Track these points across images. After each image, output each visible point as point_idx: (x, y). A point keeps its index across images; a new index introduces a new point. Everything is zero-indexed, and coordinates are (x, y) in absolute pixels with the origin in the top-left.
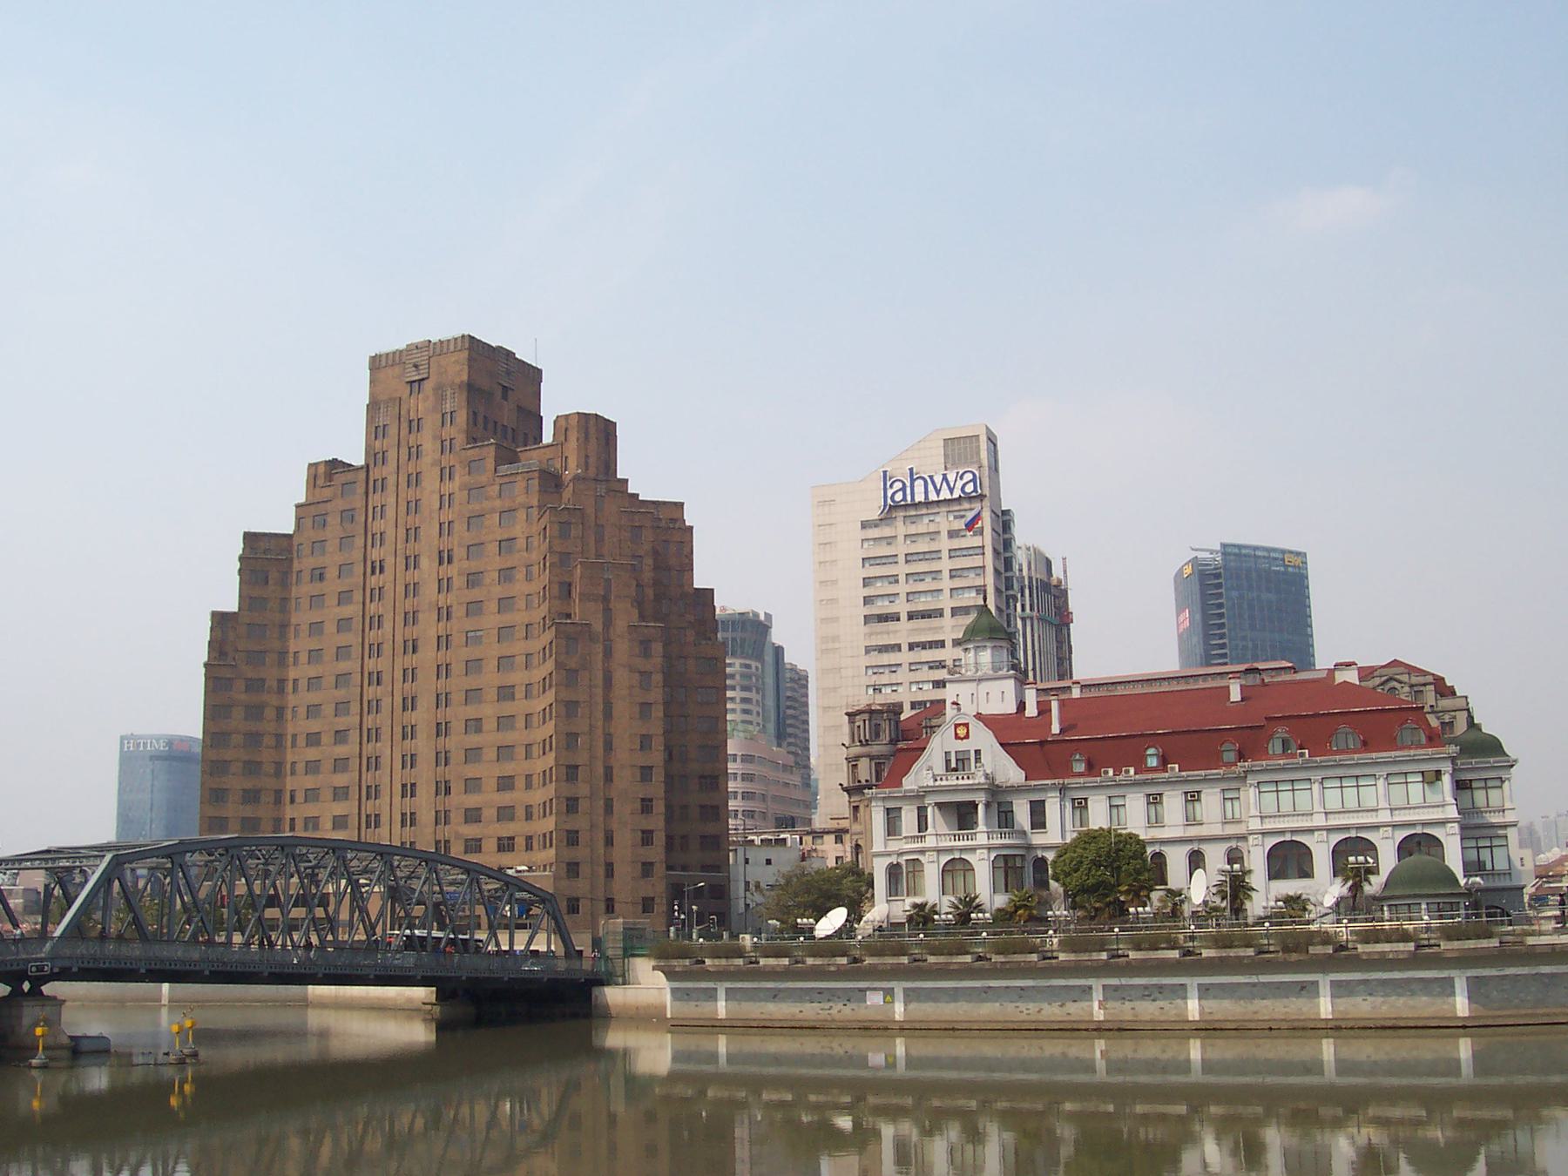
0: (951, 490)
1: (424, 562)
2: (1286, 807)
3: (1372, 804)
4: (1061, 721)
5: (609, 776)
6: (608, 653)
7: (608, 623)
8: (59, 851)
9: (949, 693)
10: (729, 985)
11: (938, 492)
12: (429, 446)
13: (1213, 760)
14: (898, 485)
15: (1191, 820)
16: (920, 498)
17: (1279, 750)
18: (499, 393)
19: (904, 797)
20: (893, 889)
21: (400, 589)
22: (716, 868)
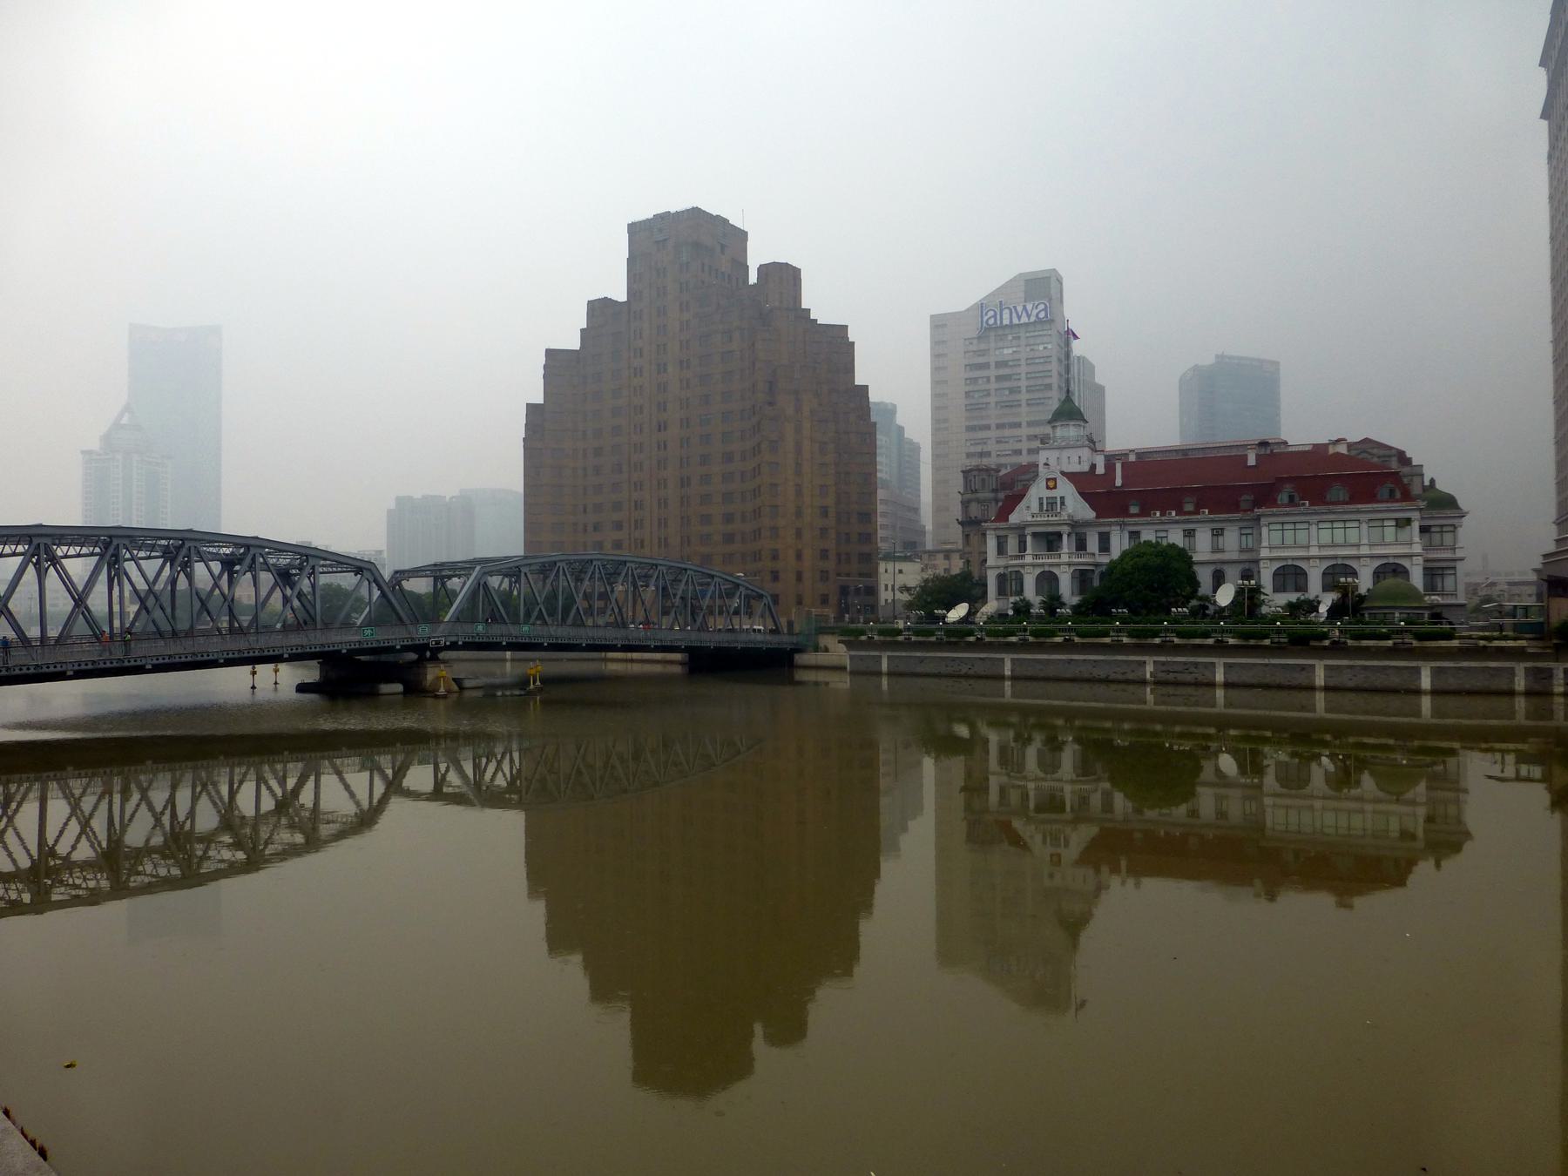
0: (1029, 316)
1: (670, 369)
2: (1289, 540)
3: (1354, 540)
4: (1123, 477)
8: (442, 564)
9: (1042, 457)
11: (1019, 318)
13: (1234, 507)
15: (1216, 549)
16: (1007, 321)
17: (1286, 500)
19: (1010, 529)
20: (1002, 592)
22: (869, 575)
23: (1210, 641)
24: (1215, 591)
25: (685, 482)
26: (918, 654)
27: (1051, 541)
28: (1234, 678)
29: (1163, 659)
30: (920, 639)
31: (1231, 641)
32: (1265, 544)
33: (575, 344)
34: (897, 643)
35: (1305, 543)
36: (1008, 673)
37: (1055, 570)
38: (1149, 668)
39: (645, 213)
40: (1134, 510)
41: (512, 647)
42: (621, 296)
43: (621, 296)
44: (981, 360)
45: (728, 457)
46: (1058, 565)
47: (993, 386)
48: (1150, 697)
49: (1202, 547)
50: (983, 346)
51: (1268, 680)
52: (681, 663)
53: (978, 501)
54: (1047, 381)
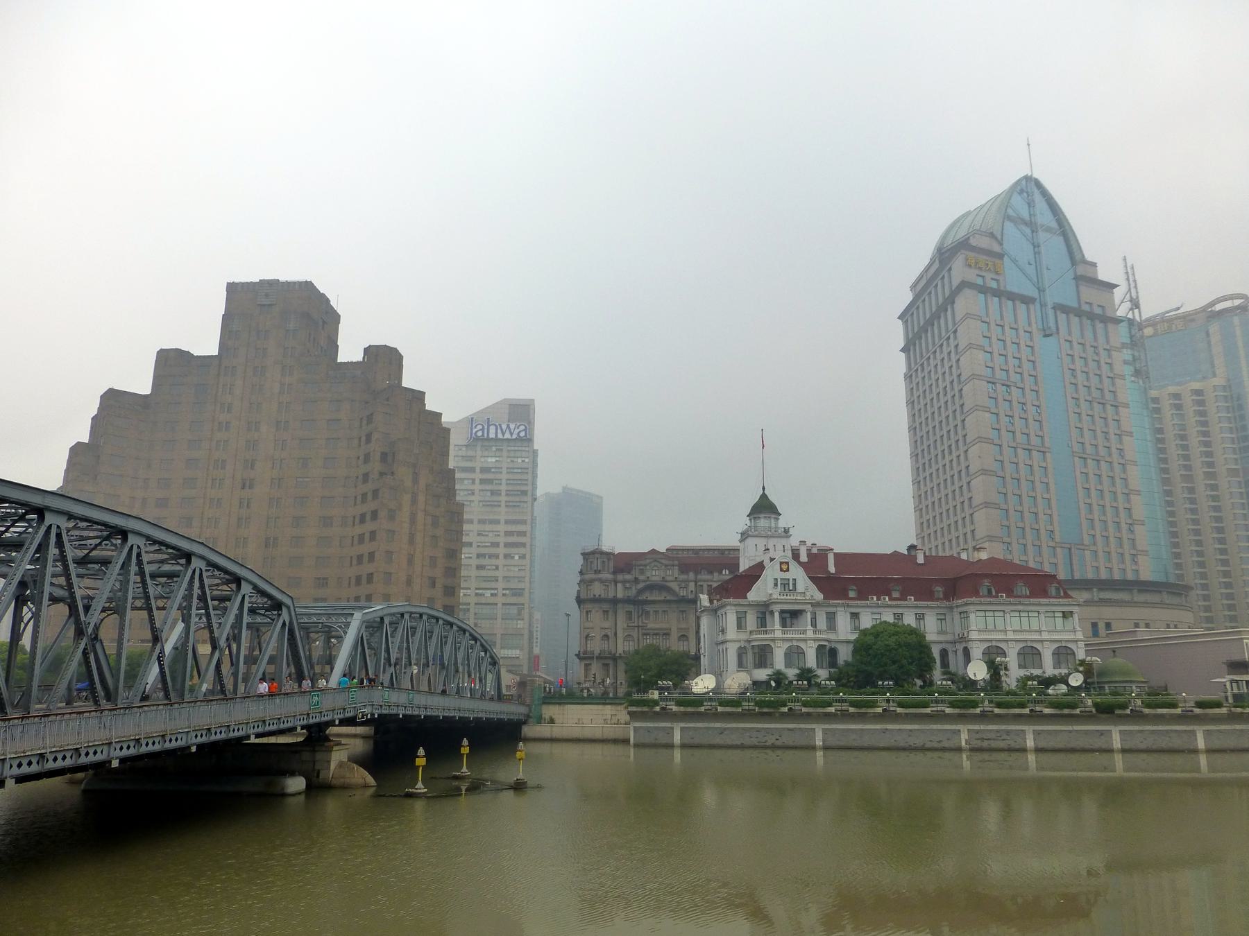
2: (991, 627)
5: (409, 582)
6: (414, 501)
7: (415, 481)
10: (683, 725)
14: (480, 427)
16: (492, 435)
17: (986, 592)
19: (750, 605)
23: (1027, 711)
24: (966, 668)
25: (269, 543)
26: (718, 725)
27: (791, 616)
28: (1042, 744)
29: (976, 727)
30: (728, 709)
31: (1047, 711)
32: (973, 628)
34: (699, 714)
35: (1002, 628)
36: (819, 743)
37: (802, 645)
38: (964, 736)
40: (852, 594)
44: (469, 464)
45: (327, 521)
47: (477, 487)
48: (966, 764)
49: (931, 629)
50: (470, 453)
51: (1073, 745)
52: (364, 737)
53: (601, 581)
54: (524, 488)
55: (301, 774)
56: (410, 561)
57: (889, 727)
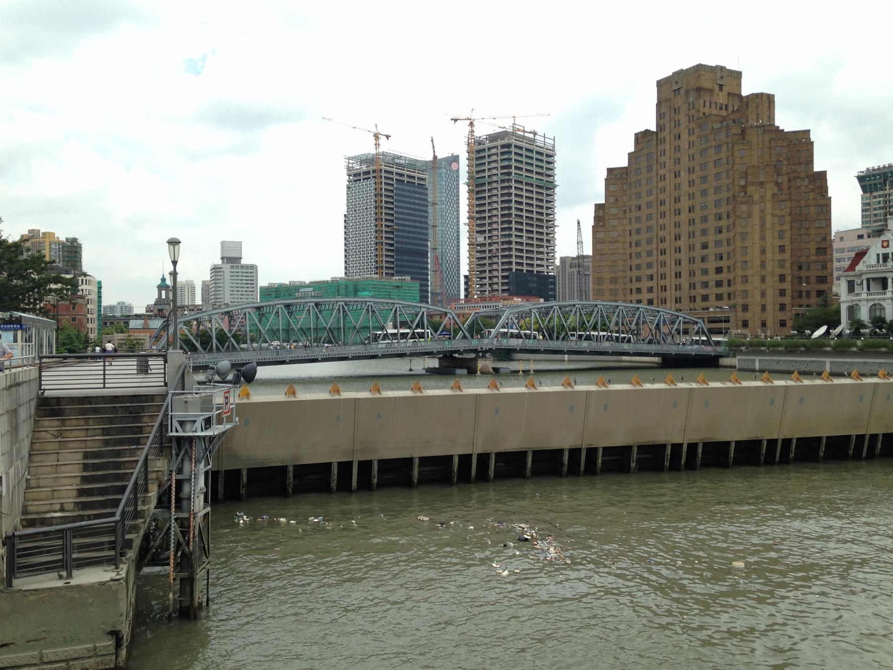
1: (682, 174)
5: (763, 265)
12: (684, 120)
18: (717, 88)
21: (673, 187)
26: (776, 358)
33: (625, 164)
34: (762, 351)
39: (667, 72)
41: (570, 352)
42: (653, 128)
43: (653, 128)
46: (884, 299)
55: (466, 368)
56: (763, 252)
57: (868, 360)
